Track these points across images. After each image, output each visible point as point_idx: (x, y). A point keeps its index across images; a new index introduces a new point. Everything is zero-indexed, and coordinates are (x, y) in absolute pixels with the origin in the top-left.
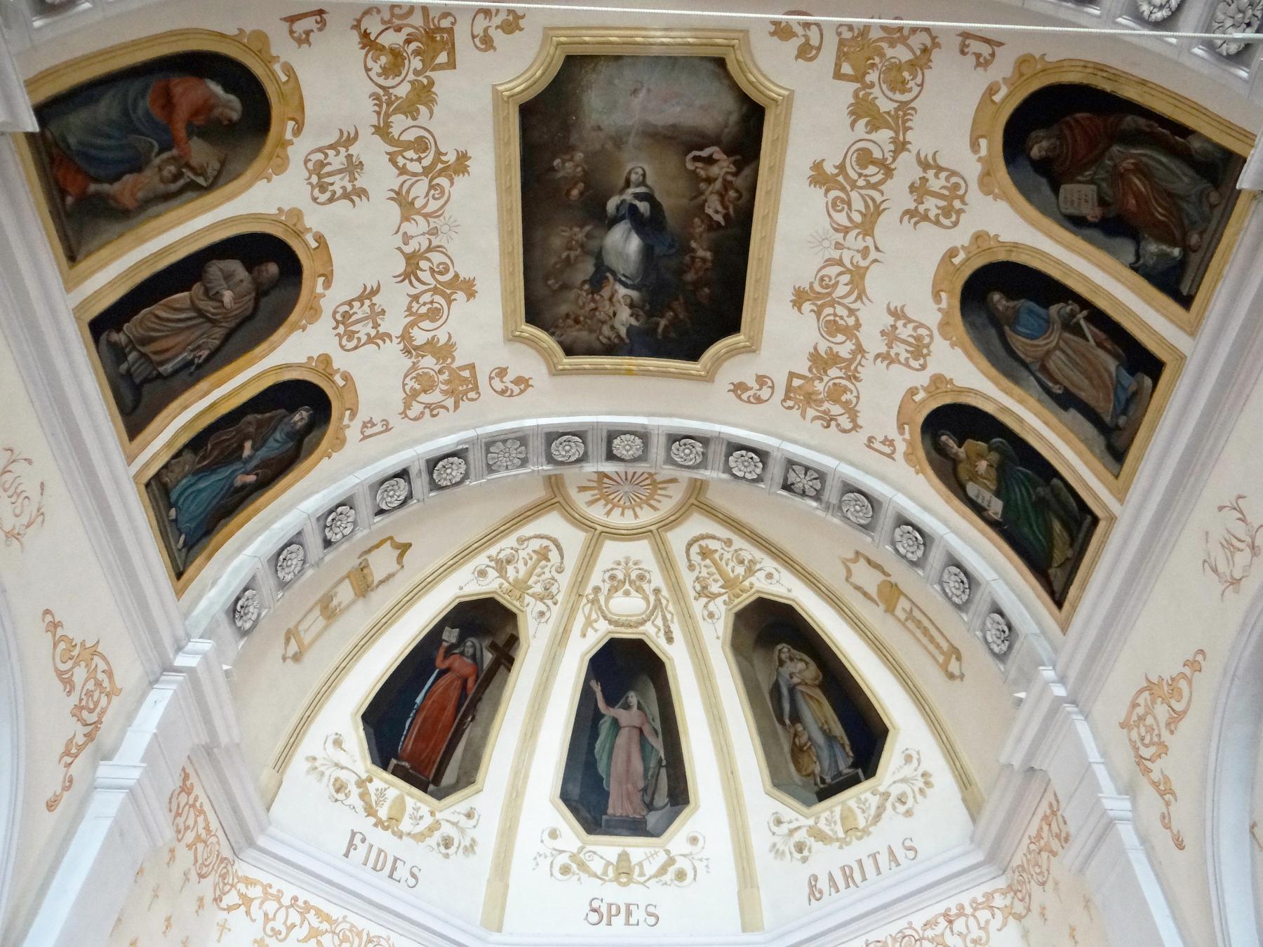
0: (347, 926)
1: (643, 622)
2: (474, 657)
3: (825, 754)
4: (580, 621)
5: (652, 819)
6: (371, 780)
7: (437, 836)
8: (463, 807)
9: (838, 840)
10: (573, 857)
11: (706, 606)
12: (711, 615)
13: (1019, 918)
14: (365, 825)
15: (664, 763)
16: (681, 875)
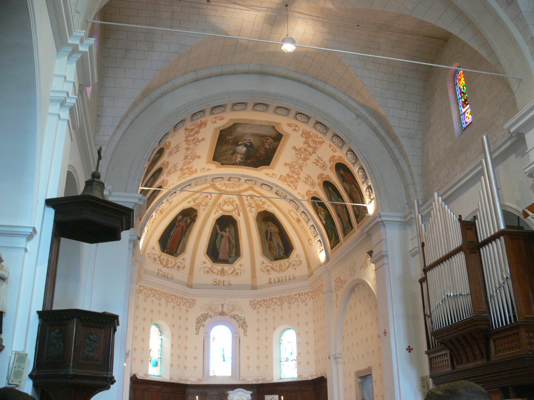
0: (160, 292)
1: (232, 211)
2: (185, 222)
3: (277, 250)
4: (214, 210)
5: (230, 260)
6: (161, 256)
7: (176, 266)
8: (181, 258)
9: (278, 271)
10: (210, 269)
11: (250, 209)
12: (251, 211)
13: (313, 299)
14: (160, 267)
15: (235, 246)
16: (237, 274)
